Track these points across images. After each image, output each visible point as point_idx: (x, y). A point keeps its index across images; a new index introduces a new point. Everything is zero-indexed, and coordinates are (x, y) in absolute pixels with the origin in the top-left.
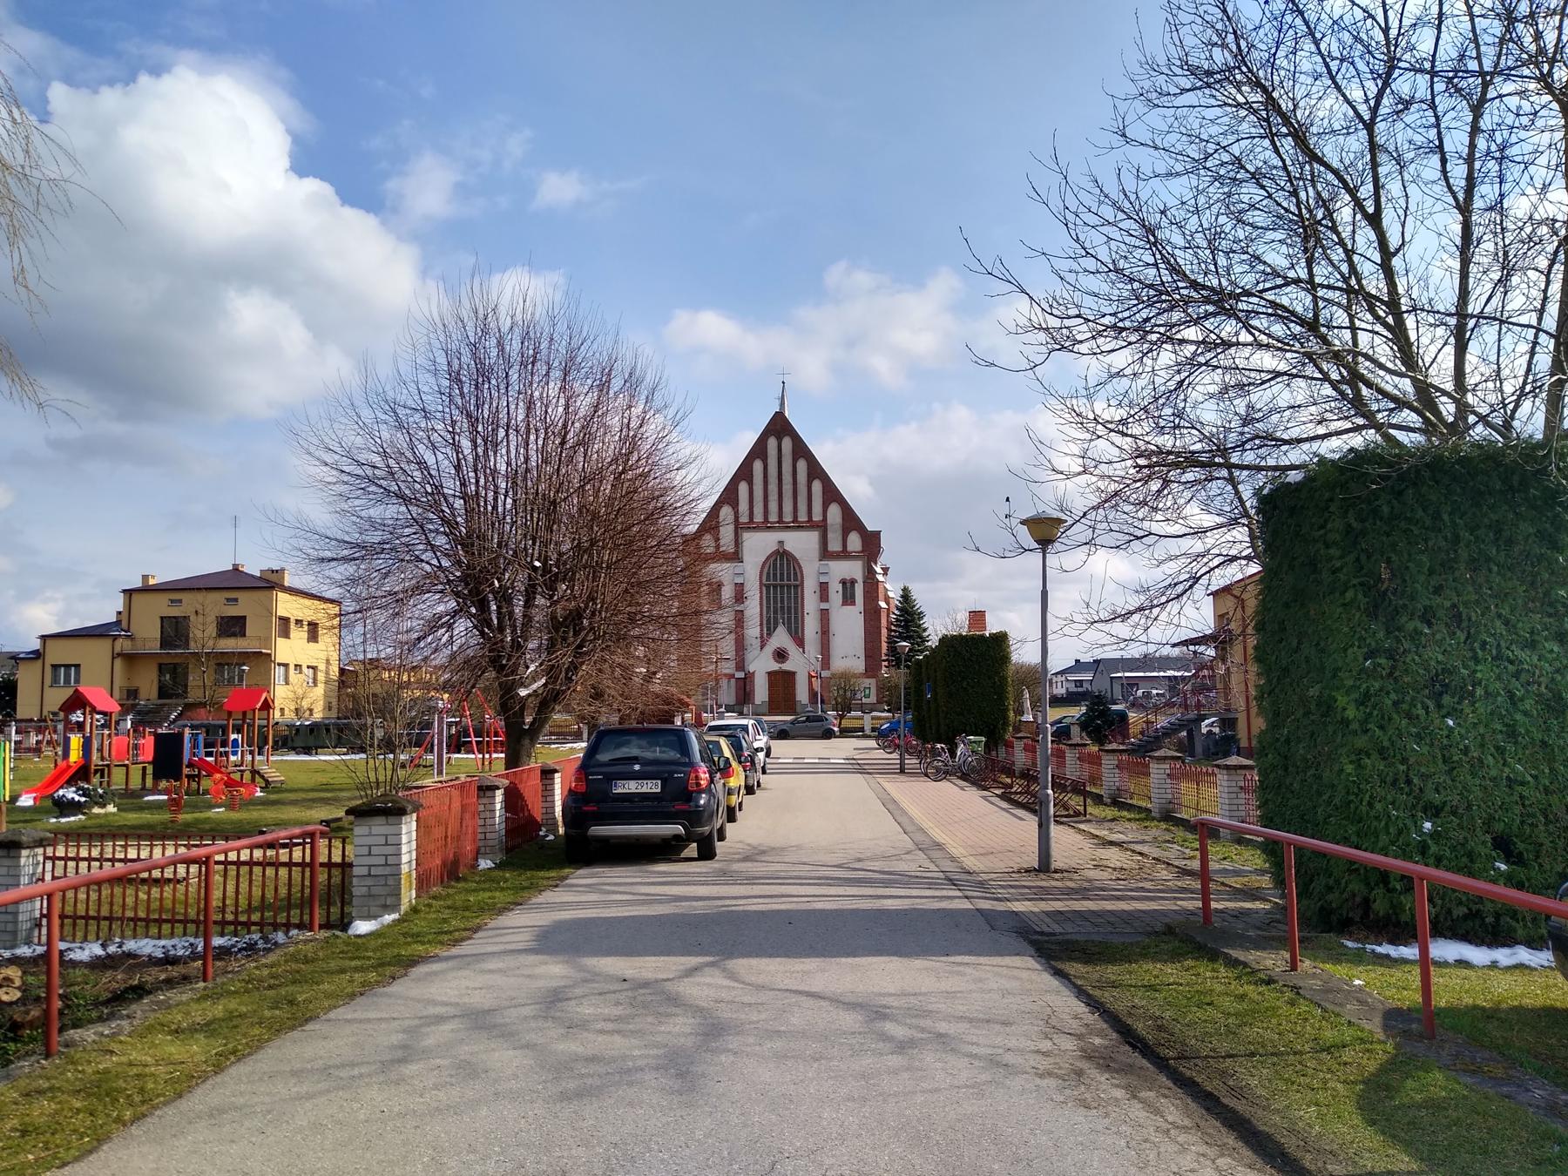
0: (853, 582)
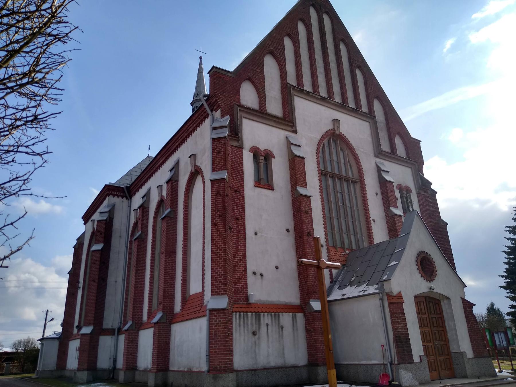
0: (258, 183)
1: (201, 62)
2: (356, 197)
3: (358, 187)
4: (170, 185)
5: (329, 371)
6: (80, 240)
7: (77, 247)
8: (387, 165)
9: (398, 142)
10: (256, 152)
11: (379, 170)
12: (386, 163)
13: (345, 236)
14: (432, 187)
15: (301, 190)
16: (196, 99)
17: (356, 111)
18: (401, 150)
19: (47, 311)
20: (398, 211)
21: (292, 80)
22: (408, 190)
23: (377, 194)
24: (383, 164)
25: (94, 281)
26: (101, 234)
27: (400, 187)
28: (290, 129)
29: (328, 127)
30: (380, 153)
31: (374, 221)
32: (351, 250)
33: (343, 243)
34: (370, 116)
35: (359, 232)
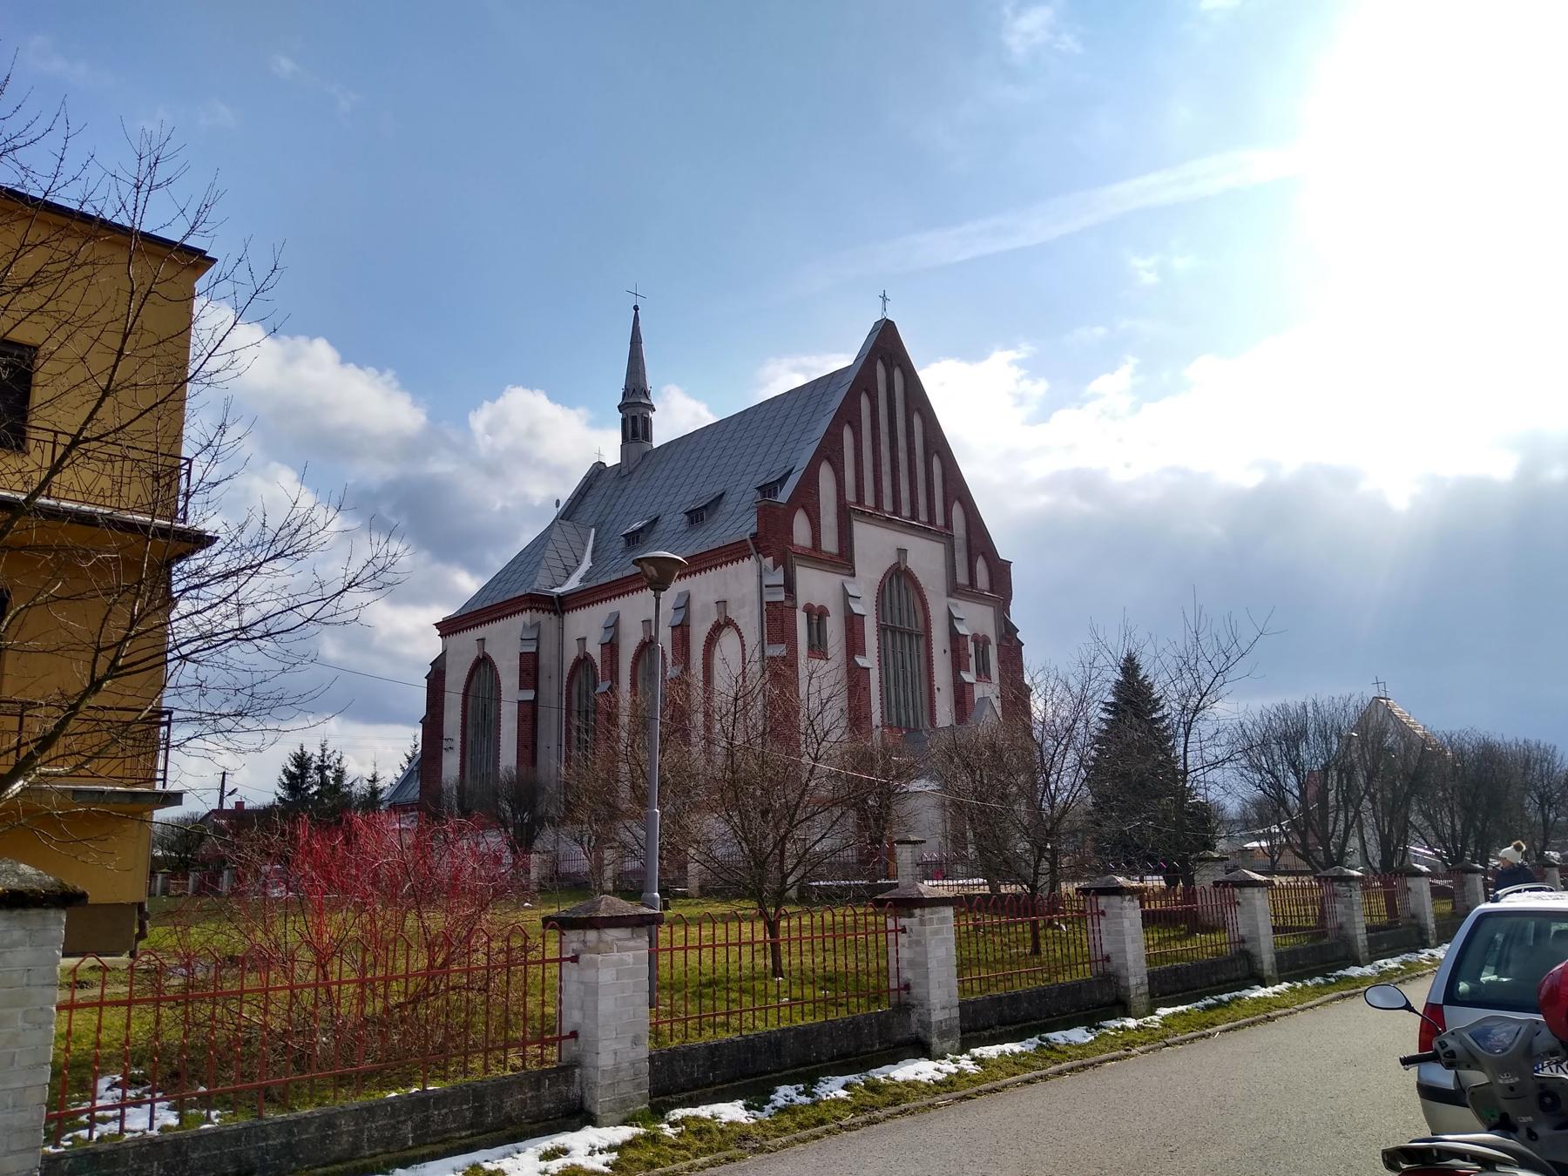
1: (636, 318)
2: (918, 656)
3: (922, 643)
4: (678, 631)
5: (580, 1021)
6: (438, 665)
7: (432, 676)
8: (964, 609)
9: (981, 566)
10: (809, 609)
11: (951, 617)
12: (961, 603)
13: (903, 711)
14: (1019, 635)
15: (860, 661)
16: (631, 400)
17: (925, 531)
18: (983, 580)
19: (224, 773)
20: (969, 677)
21: (850, 496)
22: (986, 641)
23: (945, 651)
24: (956, 606)
25: (526, 747)
26: (529, 674)
27: (976, 638)
28: (847, 571)
29: (889, 560)
30: (954, 591)
31: (938, 689)
32: (909, 729)
33: (899, 720)
34: (944, 535)
35: (919, 708)
